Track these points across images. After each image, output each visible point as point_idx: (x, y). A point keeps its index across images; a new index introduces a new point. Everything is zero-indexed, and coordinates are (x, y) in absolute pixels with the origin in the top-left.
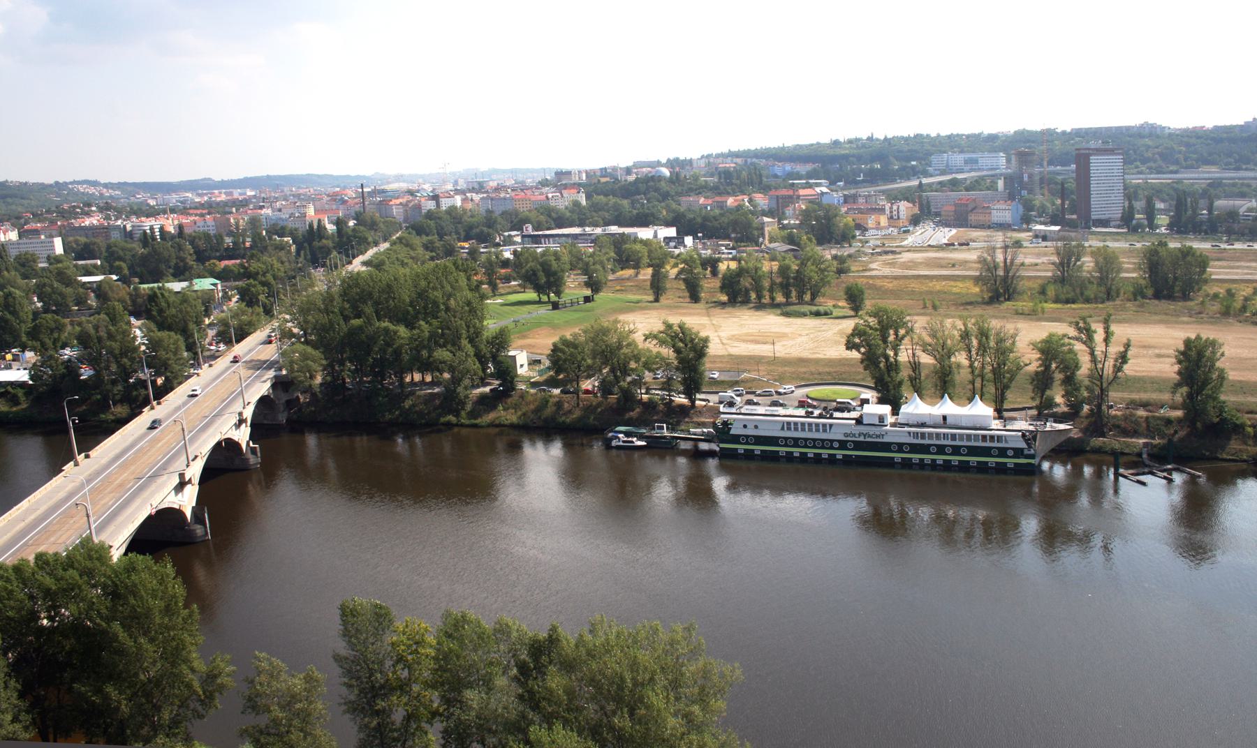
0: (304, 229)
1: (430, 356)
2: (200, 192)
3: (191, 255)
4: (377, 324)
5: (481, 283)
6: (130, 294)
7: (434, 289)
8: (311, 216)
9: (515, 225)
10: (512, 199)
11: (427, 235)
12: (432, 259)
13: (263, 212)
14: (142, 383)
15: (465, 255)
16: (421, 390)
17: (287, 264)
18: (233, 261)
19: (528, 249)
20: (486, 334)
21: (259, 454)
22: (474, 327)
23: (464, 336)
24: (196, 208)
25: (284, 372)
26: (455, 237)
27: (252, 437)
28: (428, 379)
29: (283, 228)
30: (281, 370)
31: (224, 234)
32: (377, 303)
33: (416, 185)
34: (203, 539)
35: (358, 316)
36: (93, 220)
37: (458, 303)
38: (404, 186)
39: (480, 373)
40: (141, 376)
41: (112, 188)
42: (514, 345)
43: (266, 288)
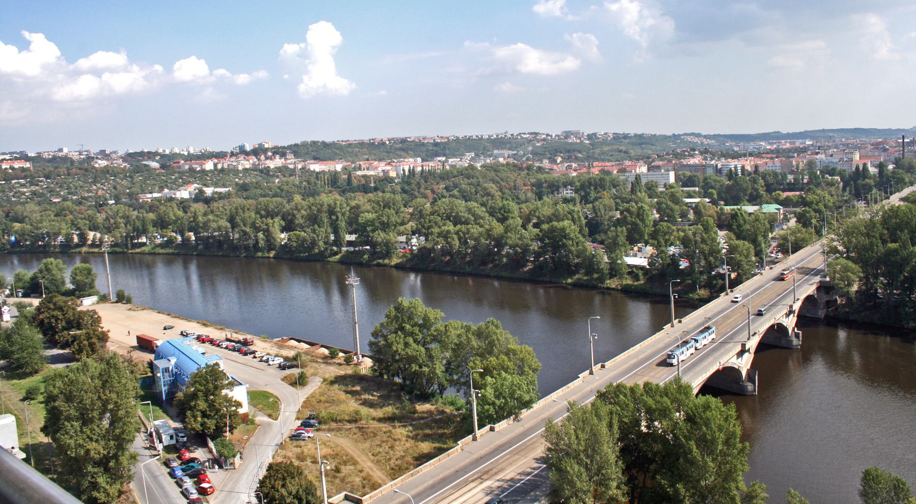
2: (771, 141)
3: (762, 187)
6: (717, 212)
14: (722, 277)
18: (793, 193)
21: (801, 339)
24: (767, 153)
25: (828, 279)
27: (797, 325)
30: (825, 277)
34: (751, 393)
35: (895, 241)
36: (696, 160)
41: (709, 138)
43: (817, 214)
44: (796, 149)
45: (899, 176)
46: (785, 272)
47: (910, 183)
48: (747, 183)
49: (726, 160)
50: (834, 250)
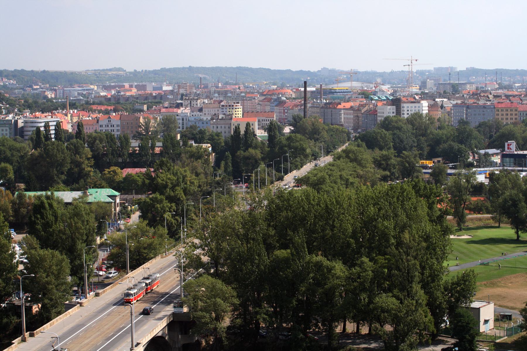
0: (227, 135)
1: (370, 302)
3: (88, 159)
4: (308, 257)
5: (446, 213)
6: (13, 203)
7: (386, 217)
8: (237, 119)
9: (494, 141)
10: (494, 107)
11: (381, 149)
12: (385, 179)
13: (179, 111)
14: (15, 310)
15: (427, 176)
16: (353, 343)
17: (202, 176)
18: (137, 170)
19: (509, 172)
20: (445, 279)
22: (431, 268)
23: (417, 279)
24: (100, 104)
25: (185, 310)
26: (417, 152)
28: (365, 330)
29: (202, 132)
30: (182, 307)
31: (130, 136)
32: (311, 231)
33: (372, 86)
35: (284, 247)
37: (414, 236)
38: (357, 85)
39: (432, 328)
40: (15, 300)
42: (479, 295)
43: (173, 204)
44: (146, 98)
45: (298, 144)
46: (132, 292)
47: (313, 155)
48: (63, 153)
49: (31, 113)
50: (196, 263)
